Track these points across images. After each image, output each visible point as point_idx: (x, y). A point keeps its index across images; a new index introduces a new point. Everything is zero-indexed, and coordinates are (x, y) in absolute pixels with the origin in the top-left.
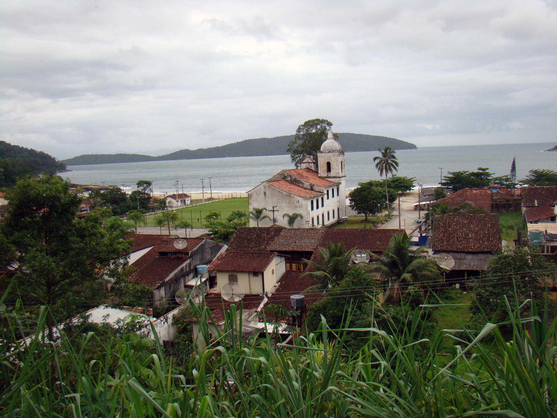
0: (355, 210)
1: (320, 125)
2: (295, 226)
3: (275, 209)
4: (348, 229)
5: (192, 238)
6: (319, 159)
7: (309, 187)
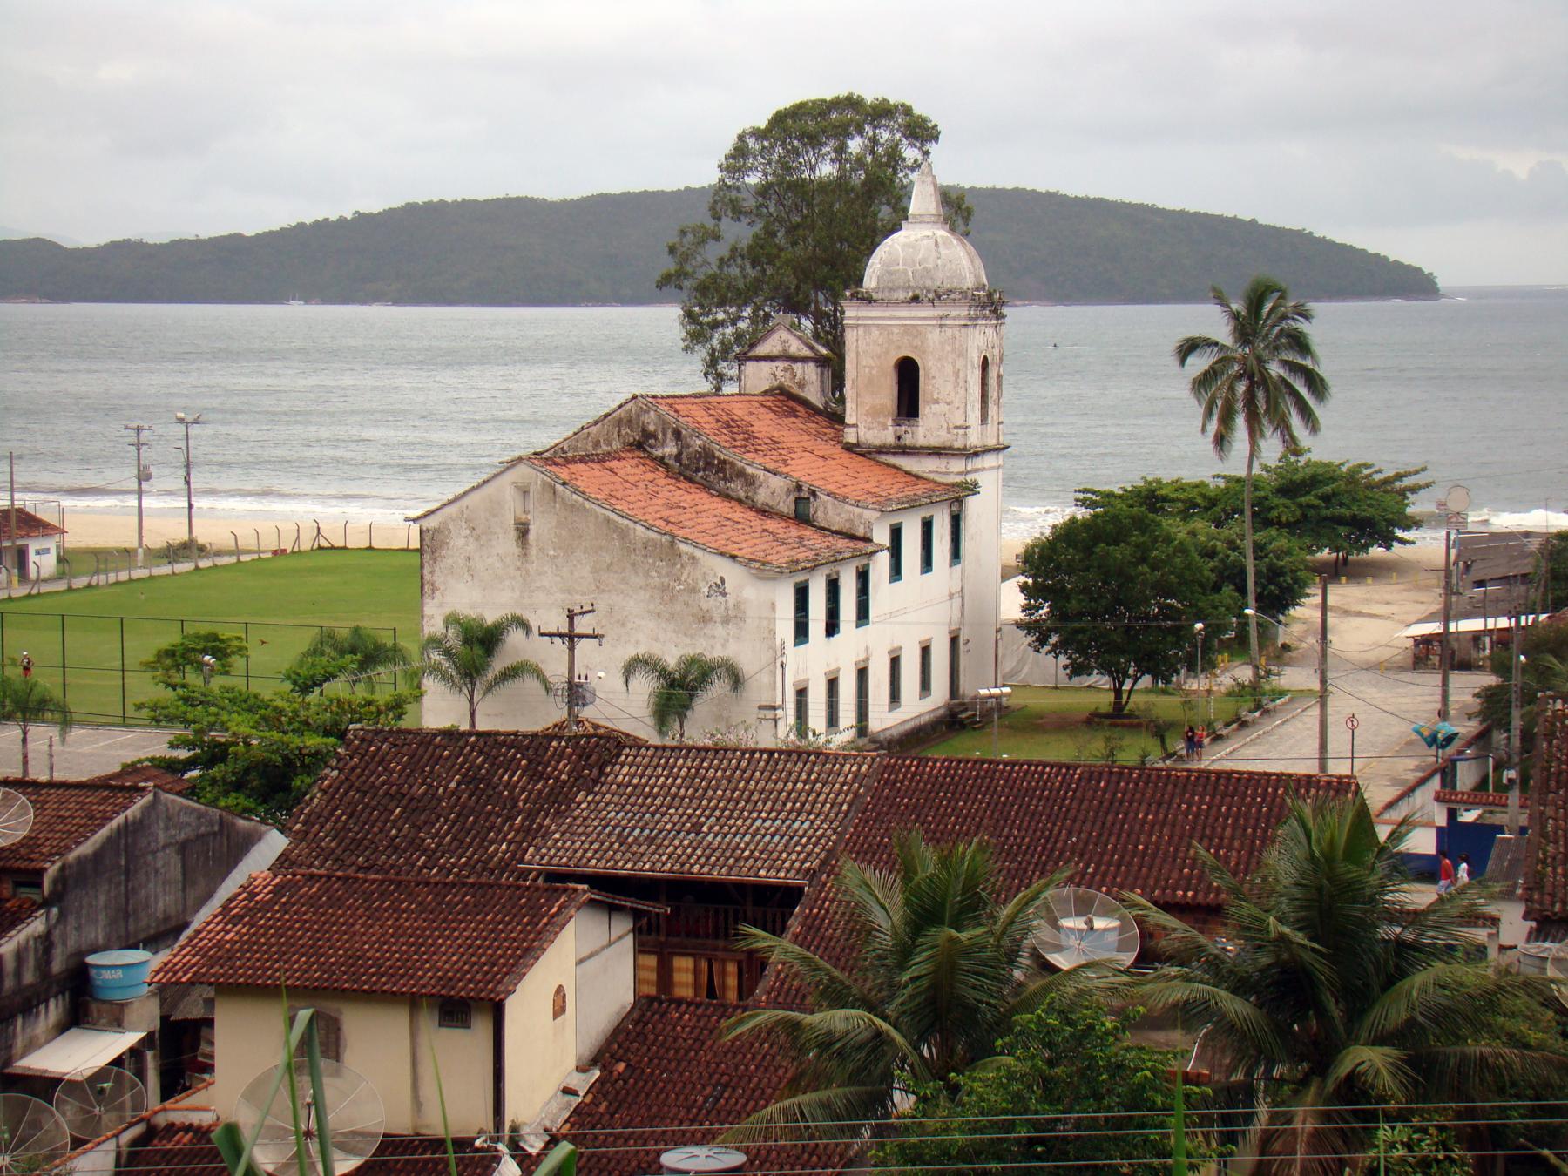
0: (1055, 651)
1: (861, 133)
2: (698, 728)
3: (582, 627)
4: (1013, 763)
5: (64, 785)
6: (850, 337)
7: (787, 506)
